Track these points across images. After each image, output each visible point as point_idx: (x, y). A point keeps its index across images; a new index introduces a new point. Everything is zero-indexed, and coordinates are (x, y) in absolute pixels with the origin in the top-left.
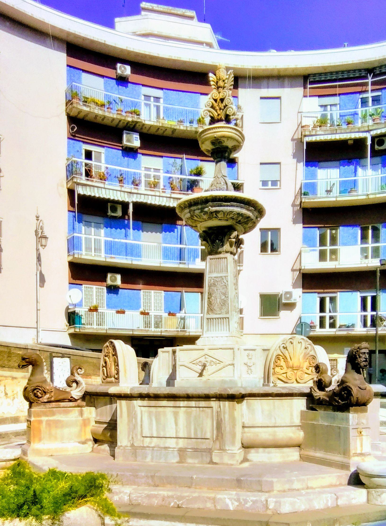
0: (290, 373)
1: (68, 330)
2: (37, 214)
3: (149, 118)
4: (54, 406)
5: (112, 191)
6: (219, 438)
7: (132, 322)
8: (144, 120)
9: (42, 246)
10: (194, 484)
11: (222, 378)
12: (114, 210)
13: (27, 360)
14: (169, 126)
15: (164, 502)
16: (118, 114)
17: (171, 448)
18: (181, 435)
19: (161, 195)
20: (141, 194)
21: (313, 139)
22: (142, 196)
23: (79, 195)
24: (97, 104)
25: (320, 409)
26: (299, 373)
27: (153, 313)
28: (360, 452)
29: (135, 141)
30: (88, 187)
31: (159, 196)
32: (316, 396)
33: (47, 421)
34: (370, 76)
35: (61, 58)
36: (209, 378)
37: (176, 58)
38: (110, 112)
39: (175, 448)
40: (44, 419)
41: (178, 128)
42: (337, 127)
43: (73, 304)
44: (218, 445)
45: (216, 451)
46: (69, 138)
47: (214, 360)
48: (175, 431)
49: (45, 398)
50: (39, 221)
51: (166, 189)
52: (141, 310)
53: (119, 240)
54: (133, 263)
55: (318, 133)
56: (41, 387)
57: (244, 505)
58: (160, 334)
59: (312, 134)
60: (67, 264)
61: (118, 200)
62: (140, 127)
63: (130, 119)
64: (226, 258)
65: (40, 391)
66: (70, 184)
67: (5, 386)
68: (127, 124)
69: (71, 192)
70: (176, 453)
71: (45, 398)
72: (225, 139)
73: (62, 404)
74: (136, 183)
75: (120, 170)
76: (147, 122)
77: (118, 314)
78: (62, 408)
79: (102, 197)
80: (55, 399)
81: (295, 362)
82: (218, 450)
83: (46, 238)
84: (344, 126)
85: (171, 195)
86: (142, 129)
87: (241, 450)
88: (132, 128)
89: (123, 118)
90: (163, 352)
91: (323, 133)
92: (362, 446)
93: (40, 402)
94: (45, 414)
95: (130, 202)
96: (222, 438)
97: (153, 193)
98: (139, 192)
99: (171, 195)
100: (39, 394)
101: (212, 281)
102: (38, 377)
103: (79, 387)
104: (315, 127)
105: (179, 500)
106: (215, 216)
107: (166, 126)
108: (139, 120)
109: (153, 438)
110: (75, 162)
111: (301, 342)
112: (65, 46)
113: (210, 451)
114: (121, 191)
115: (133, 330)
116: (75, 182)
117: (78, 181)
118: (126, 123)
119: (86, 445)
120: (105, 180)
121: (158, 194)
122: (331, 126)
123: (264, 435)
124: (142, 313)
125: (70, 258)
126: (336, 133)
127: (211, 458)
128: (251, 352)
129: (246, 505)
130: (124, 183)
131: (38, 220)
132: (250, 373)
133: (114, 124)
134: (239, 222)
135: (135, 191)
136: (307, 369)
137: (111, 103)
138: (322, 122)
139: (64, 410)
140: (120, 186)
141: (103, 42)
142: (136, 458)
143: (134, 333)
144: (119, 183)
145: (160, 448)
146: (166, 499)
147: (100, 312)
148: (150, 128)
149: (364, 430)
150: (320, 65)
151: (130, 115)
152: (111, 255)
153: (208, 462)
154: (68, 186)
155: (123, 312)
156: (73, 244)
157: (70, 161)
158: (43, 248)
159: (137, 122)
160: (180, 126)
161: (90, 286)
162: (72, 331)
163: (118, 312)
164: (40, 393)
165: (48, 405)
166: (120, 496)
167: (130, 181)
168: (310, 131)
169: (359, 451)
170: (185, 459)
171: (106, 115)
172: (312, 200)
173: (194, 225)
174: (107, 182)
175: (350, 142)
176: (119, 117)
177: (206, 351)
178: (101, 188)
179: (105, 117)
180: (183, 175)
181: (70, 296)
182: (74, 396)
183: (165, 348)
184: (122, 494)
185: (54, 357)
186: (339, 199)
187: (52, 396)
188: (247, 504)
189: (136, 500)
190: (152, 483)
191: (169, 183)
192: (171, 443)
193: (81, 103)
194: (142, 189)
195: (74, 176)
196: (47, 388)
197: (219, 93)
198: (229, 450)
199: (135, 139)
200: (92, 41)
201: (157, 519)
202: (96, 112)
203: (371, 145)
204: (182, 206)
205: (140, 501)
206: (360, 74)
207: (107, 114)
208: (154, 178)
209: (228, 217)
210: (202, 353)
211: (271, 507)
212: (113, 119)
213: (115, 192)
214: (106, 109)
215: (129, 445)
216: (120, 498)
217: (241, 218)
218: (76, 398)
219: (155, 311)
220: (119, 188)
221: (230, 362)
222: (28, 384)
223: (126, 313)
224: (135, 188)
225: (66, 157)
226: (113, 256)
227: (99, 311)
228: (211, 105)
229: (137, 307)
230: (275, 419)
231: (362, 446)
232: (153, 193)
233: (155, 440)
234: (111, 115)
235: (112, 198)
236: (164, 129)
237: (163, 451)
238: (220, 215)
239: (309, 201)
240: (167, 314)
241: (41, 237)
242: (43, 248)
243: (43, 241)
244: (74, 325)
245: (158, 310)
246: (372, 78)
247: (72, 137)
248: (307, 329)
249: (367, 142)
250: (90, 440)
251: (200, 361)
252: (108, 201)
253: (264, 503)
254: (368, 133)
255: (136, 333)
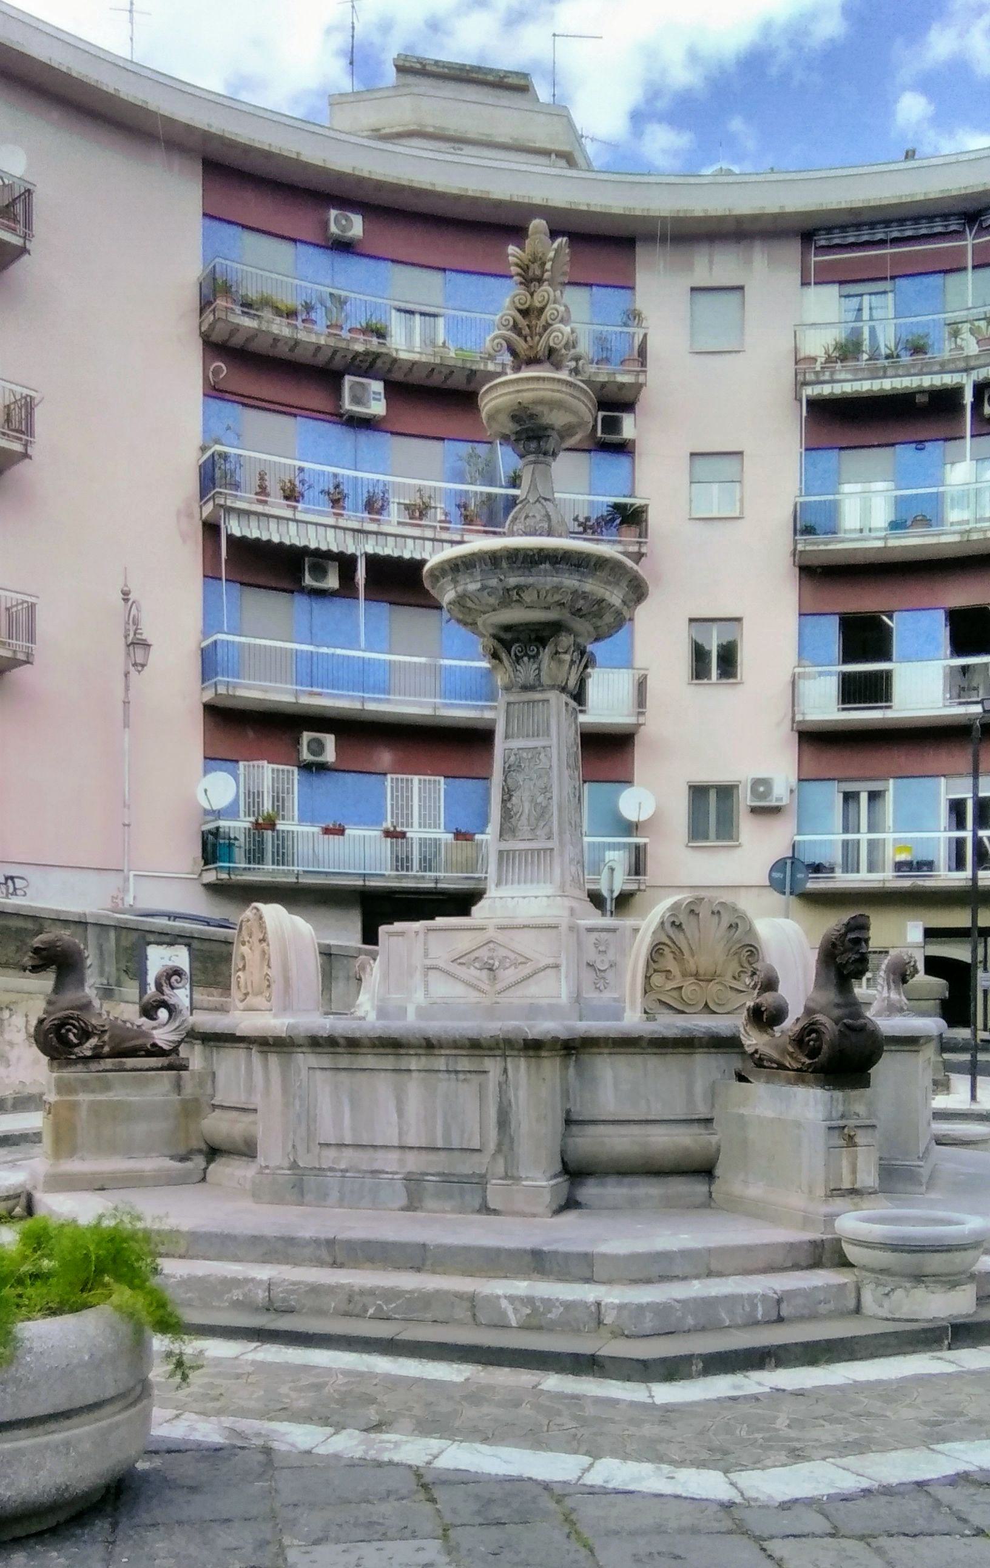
0: (690, 988)
1: (200, 875)
2: (126, 585)
3: (406, 342)
4: (109, 1067)
5: (333, 530)
6: (505, 1148)
7: (361, 854)
8: (397, 350)
9: (135, 665)
10: (429, 1262)
11: (529, 1001)
12: (320, 572)
13: (44, 953)
14: (459, 364)
15: (351, 1306)
16: (330, 335)
17: (387, 1173)
18: (411, 1141)
19: (437, 537)
20: (387, 535)
21: (826, 390)
22: (389, 538)
23: (230, 538)
24: (278, 312)
25: (758, 1079)
26: (713, 987)
27: (415, 833)
28: (849, 1186)
29: (373, 403)
30: (252, 517)
31: (433, 540)
32: (749, 1046)
33: (92, 1102)
34: (971, 231)
35: (183, 194)
36: (498, 1000)
37: (478, 195)
38: (310, 331)
39: (397, 1173)
40: (84, 1098)
41: (482, 367)
42: (886, 362)
43: (214, 811)
44: (500, 1169)
45: (494, 1181)
46: (205, 395)
47: (512, 956)
48: (397, 1130)
49: (87, 1049)
50: (130, 602)
51: (450, 522)
52: (388, 824)
53: (331, 651)
54: (366, 707)
55: (838, 377)
56: (78, 1019)
57: (543, 1314)
58: (432, 885)
59: (822, 378)
60: (202, 707)
61: (329, 552)
62: (388, 366)
63: (359, 347)
64: (548, 701)
65: (75, 1031)
66: (209, 508)
67: (27, 1016)
68: (354, 358)
69: (211, 529)
70: (399, 1185)
71: (87, 1049)
72: (545, 410)
73: (130, 1062)
74: (374, 506)
75: (335, 475)
76: (403, 355)
77: (326, 836)
78: (130, 1070)
79: (288, 542)
80: (112, 1049)
81: (703, 962)
82: (500, 1179)
83: (146, 645)
84: (906, 359)
85: (462, 536)
86: (390, 371)
87: (560, 1180)
88: (367, 365)
89: (343, 345)
90: (391, 934)
91: (849, 377)
92: (854, 1172)
93: (73, 1057)
94: (85, 1086)
95: (358, 554)
96: (512, 1149)
97: (416, 532)
98: (385, 529)
99: (462, 536)
100: (71, 1036)
101: (512, 758)
102: (70, 996)
103: (175, 1020)
104: (829, 360)
105: (388, 1301)
106: (516, 597)
107: (452, 363)
108: (383, 350)
109: (344, 1149)
110: (220, 455)
111: (719, 912)
112: (199, 168)
113: (480, 1181)
114: (335, 527)
115: (365, 875)
116: (221, 506)
117: (229, 503)
118: (350, 356)
119: (189, 1165)
120: (298, 501)
121: (429, 534)
122: (870, 359)
123: (619, 1142)
124: (388, 834)
125: (208, 696)
126: (885, 377)
127: (484, 1199)
128: (604, 935)
129: (549, 1316)
130: (344, 508)
131: (126, 600)
132: (602, 987)
133: (321, 359)
134: (578, 613)
135: (373, 527)
136: (734, 978)
137: (313, 308)
138: (848, 351)
139: (134, 1077)
140: (335, 514)
141: (294, 156)
142: (303, 1196)
143: (367, 883)
144: (333, 507)
145: (359, 1172)
146: (357, 1298)
147: (283, 831)
148: (411, 369)
149: (859, 1132)
150: (843, 206)
151: (362, 337)
152: (309, 689)
153: (477, 1207)
154: (204, 515)
155: (341, 831)
156: (209, 662)
157: (209, 453)
158: (139, 672)
159: (378, 355)
160: (486, 365)
161: (432, 778)
162: (210, 877)
163: (327, 831)
164: (74, 1034)
165: (94, 1066)
166: (246, 1289)
167: (361, 504)
168: (817, 373)
169: (846, 1185)
170: (420, 1201)
171: (299, 336)
172: (822, 547)
173: (470, 621)
174: (300, 506)
175: (921, 399)
176: (332, 342)
177: (491, 933)
178: (288, 519)
179: (297, 343)
180: (496, 486)
181: (206, 791)
182: (160, 1043)
183: (396, 924)
184: (251, 1285)
185: (149, 943)
186: (892, 543)
187: (104, 1042)
188: (550, 1312)
189: (284, 1300)
190: (329, 1259)
191: (459, 506)
192: (389, 1161)
193: (238, 309)
194: (393, 519)
195: (217, 490)
196: (94, 1022)
197: (532, 295)
198: (527, 1178)
199: (372, 396)
200: (268, 155)
201: (328, 1348)
202: (276, 332)
203: (973, 404)
204: (437, 573)
205: (293, 1303)
206: (946, 226)
207: (302, 336)
208: (412, 493)
209: (550, 599)
210: (480, 937)
211: (608, 1320)
212: (319, 348)
213: (321, 530)
214: (299, 323)
215: (286, 1164)
216: (245, 1295)
217: (582, 602)
218: (166, 1047)
219: (422, 829)
220: (331, 521)
221: (551, 961)
222: (46, 1012)
223: (347, 832)
224: (371, 519)
225: (198, 441)
226: (315, 689)
227: (278, 827)
228: (511, 323)
229: (375, 819)
230: (648, 1101)
231: (854, 1172)
232: (416, 532)
233: (348, 1153)
234: (315, 335)
235: (313, 545)
236: (445, 371)
237: (368, 1181)
238: (528, 597)
239: (815, 548)
240: (451, 836)
241: (132, 643)
242: (139, 672)
243: (139, 653)
244: (214, 862)
245: (430, 827)
246: (974, 239)
247: (214, 391)
248: (800, 876)
249: (963, 398)
250: (200, 1151)
251: (477, 958)
252: (305, 551)
253: (593, 1309)
254: (965, 374)
255: (372, 884)
